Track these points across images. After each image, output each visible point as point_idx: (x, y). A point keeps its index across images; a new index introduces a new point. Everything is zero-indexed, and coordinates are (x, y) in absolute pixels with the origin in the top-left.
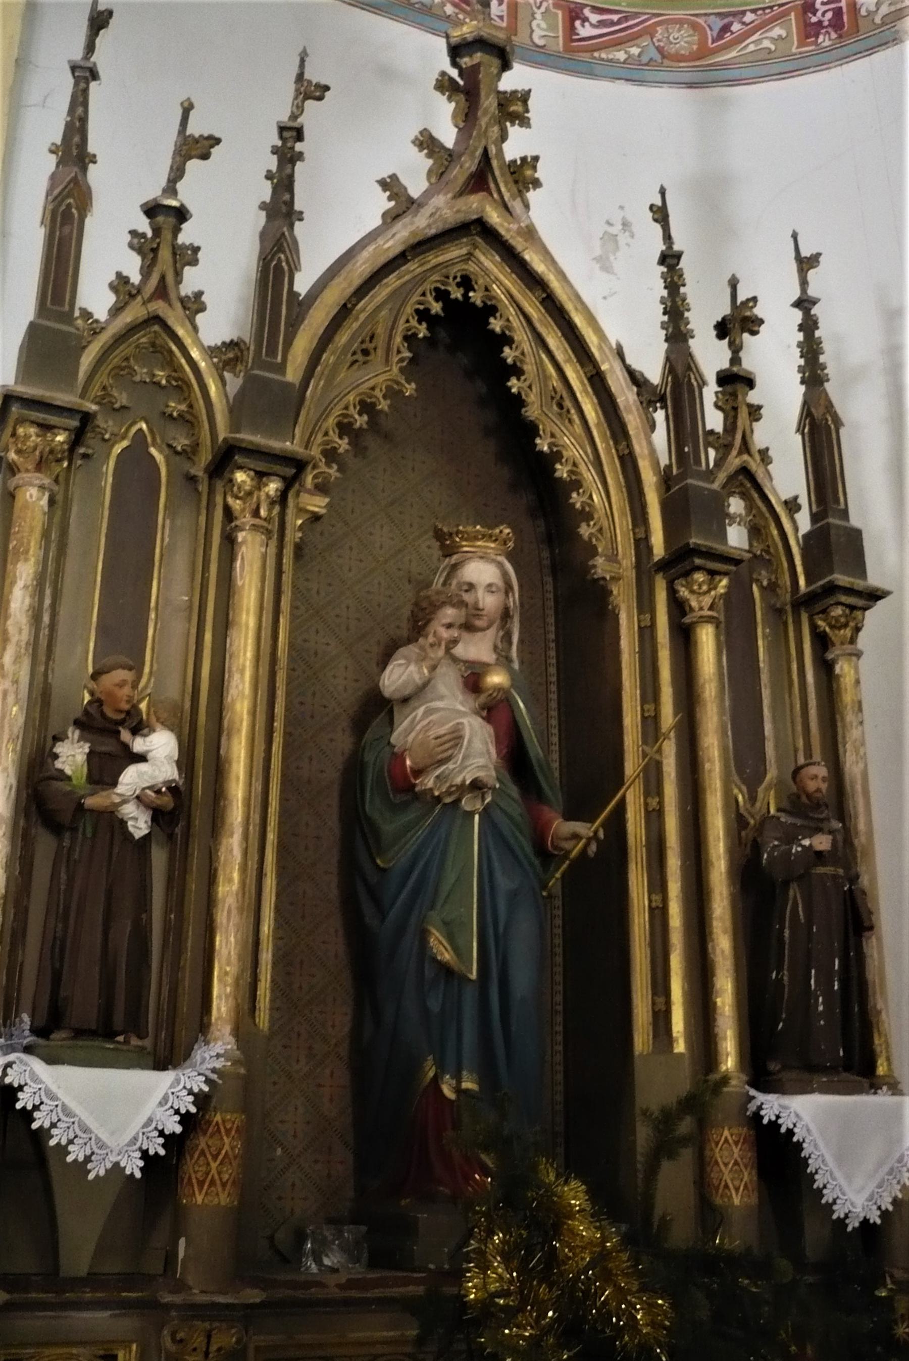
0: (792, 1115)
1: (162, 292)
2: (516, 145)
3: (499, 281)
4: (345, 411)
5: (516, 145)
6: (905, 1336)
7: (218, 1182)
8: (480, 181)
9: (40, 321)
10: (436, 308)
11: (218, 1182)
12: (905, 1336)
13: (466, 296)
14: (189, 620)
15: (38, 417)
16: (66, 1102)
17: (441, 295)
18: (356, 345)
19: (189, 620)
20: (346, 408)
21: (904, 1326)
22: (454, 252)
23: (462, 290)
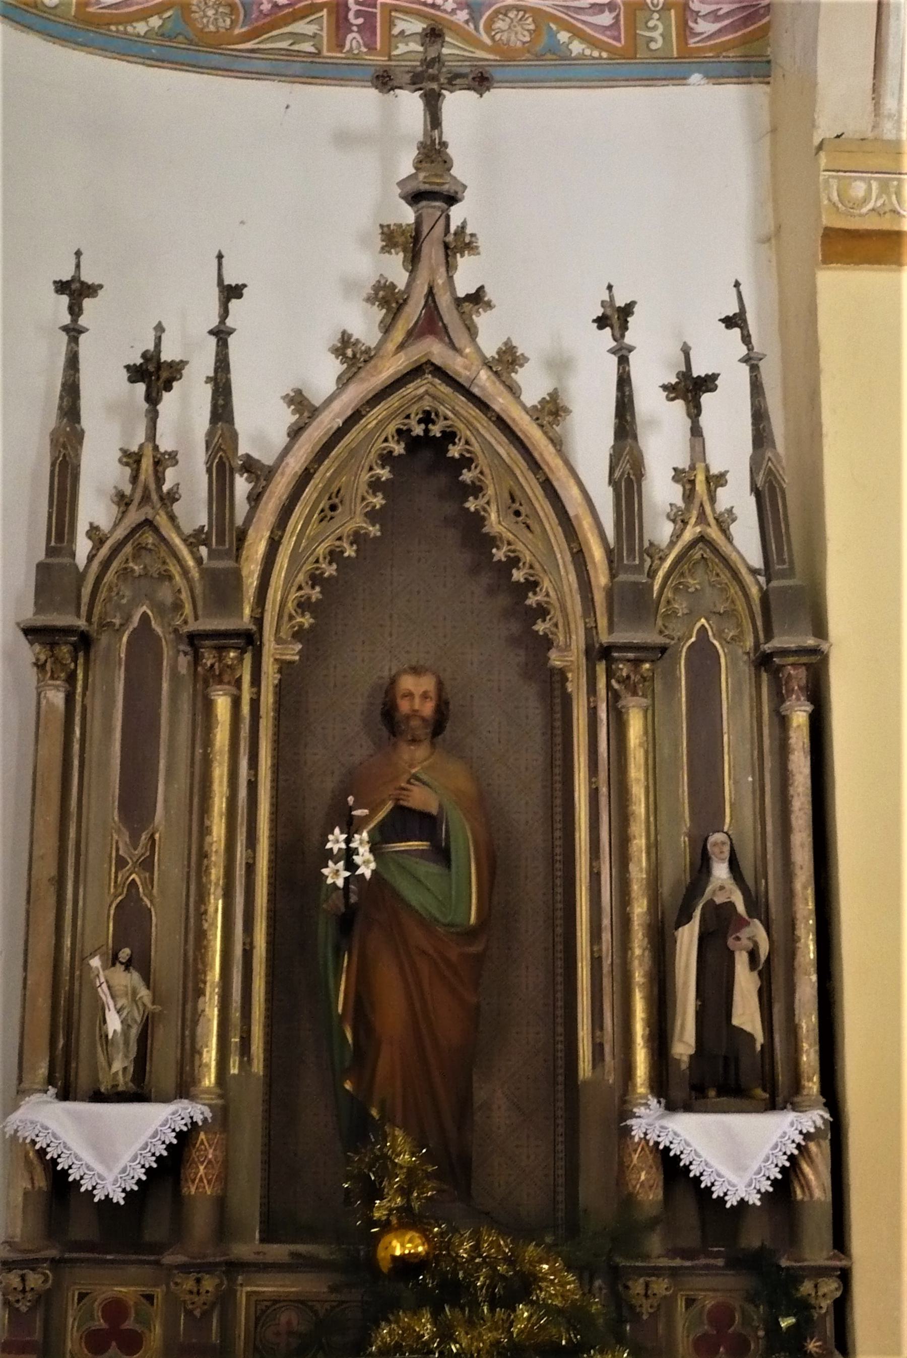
0: (671, 1133)
1: (146, 499)
2: (467, 276)
3: (455, 410)
4: (315, 565)
5: (467, 276)
6: (817, 1350)
7: (155, 497)
8: (431, 323)
9: (49, 560)
10: (384, 474)
11: (155, 497)
12: (817, 1350)
13: (427, 431)
14: (154, 980)
15: (241, 875)
16: (100, 1172)
17: (402, 434)
18: (323, 502)
19: (154, 980)
20: (317, 561)
21: (818, 1344)
22: (411, 389)
23: (423, 426)
